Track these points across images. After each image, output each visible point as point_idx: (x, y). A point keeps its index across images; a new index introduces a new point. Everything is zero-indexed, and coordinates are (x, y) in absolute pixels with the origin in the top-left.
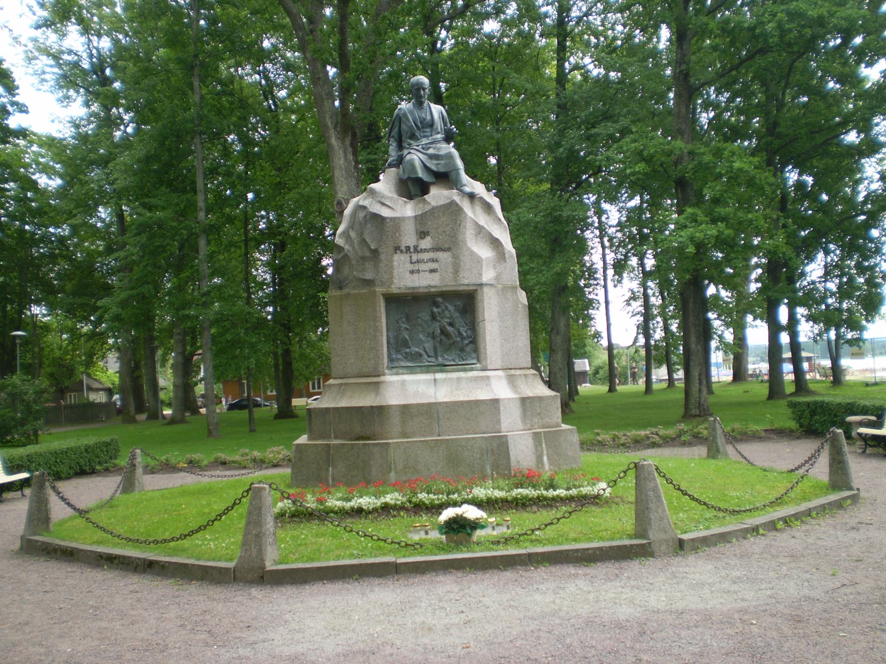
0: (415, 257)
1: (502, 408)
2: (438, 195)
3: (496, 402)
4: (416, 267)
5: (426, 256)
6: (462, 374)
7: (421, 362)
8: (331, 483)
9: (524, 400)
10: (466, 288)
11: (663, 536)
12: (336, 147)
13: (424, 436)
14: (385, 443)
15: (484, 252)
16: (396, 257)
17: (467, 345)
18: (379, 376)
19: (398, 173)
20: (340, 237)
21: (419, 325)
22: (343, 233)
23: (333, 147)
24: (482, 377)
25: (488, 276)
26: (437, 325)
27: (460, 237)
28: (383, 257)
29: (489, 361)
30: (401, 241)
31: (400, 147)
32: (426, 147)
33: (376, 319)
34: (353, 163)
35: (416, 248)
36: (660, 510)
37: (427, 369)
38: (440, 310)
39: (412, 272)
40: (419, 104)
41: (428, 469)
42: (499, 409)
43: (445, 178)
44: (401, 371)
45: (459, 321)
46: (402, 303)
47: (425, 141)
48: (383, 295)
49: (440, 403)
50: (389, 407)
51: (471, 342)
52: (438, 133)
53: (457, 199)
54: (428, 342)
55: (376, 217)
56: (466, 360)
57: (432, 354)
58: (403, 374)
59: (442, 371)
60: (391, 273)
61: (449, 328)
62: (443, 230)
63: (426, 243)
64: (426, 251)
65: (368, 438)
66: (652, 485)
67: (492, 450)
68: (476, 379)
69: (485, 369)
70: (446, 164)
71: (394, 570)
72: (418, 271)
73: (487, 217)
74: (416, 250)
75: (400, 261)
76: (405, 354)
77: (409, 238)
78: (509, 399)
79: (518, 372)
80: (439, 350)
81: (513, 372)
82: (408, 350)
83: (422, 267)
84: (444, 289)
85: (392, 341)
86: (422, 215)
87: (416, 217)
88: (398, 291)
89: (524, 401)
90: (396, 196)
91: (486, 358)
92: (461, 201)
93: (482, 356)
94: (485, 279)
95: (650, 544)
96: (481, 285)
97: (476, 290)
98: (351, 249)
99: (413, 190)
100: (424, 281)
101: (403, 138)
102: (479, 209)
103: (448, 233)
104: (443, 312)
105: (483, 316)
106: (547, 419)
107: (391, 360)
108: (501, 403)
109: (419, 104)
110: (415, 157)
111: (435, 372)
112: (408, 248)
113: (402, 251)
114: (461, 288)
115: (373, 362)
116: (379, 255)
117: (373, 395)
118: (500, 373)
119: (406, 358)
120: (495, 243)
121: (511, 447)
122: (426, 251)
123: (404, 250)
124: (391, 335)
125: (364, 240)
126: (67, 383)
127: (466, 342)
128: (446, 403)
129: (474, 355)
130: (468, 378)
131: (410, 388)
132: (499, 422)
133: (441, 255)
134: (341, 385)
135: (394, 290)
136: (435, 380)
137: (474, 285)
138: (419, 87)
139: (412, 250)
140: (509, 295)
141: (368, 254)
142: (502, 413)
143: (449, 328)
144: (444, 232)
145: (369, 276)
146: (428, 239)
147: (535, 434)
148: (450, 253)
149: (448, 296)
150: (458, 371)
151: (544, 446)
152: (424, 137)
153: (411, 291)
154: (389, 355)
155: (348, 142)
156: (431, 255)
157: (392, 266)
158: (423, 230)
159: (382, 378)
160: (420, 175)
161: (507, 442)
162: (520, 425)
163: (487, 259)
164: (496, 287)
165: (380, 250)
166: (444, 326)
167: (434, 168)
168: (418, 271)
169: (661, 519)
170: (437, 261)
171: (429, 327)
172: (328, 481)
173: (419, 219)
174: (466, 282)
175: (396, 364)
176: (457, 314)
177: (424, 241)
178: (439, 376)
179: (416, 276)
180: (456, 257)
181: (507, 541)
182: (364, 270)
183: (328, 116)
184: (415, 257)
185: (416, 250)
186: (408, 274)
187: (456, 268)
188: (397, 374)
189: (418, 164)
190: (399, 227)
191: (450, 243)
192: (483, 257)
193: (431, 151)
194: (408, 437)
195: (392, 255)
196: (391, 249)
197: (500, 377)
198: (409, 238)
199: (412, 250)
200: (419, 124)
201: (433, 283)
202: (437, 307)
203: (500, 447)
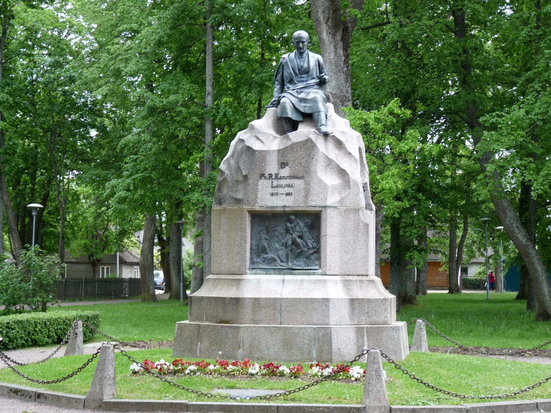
0: (275, 183)
1: (331, 306)
2: (305, 131)
3: (326, 301)
4: (275, 191)
6: (305, 277)
7: (275, 265)
8: (198, 354)
9: (352, 301)
10: (313, 209)
11: (376, 404)
12: (327, 42)
13: (269, 323)
14: (237, 327)
15: (330, 180)
16: (261, 182)
17: (312, 254)
18: (242, 274)
19: (276, 112)
20: (224, 163)
21: (276, 236)
22: (227, 160)
23: (324, 42)
24: (320, 280)
25: (332, 199)
26: (289, 236)
27: (312, 168)
28: (251, 181)
29: (328, 268)
30: (265, 170)
31: (282, 90)
32: (300, 91)
33: (244, 230)
34: (343, 58)
35: (276, 175)
36: (378, 386)
37: (280, 271)
38: (292, 225)
39: (272, 194)
40: (301, 54)
41: (268, 349)
43: (309, 117)
44: (259, 272)
45: (307, 235)
46: (263, 219)
47: (301, 85)
48: (249, 211)
49: (283, 299)
50: (244, 299)
51: (315, 252)
52: (314, 78)
53: (313, 137)
54: (282, 250)
55: (249, 148)
56: (311, 266)
57: (285, 260)
58: (260, 274)
59: (290, 274)
60: (256, 195)
61: (299, 240)
62: (298, 160)
63: (285, 172)
64: (284, 178)
65: (227, 322)
66: (375, 367)
67: (319, 338)
68: (316, 281)
69: (324, 274)
70: (311, 107)
71: (186, 409)
72: (277, 194)
73: (337, 152)
74: (277, 177)
75: (264, 186)
76: (261, 258)
77: (272, 168)
78: (339, 299)
79: (356, 278)
80: (290, 256)
81: (350, 278)
82: (265, 256)
83: (280, 190)
84: (296, 209)
85: (254, 248)
86: (284, 149)
87: (279, 150)
88: (261, 209)
89: (354, 303)
90: (273, 132)
92: (316, 139)
93: (323, 264)
94: (329, 203)
95: (364, 408)
96: (325, 207)
97: (321, 211)
98: (229, 173)
99: (286, 127)
100: (281, 202)
101: (285, 82)
102: (331, 145)
103: (303, 164)
104: (295, 227)
106: (374, 317)
107: (252, 263)
108: (331, 302)
109: (301, 54)
110: (288, 100)
111: (285, 274)
112: (270, 175)
113: (265, 178)
114: (309, 209)
115: (238, 263)
116: (248, 179)
117: (235, 288)
118: (338, 278)
119: (264, 261)
120: (342, 173)
121: (334, 337)
122: (284, 178)
124: (254, 243)
125: (239, 167)
126: (100, 256)
127: (311, 252)
128: (288, 299)
129: (317, 263)
130: (309, 281)
131: (263, 285)
132: (328, 317)
133: (296, 182)
134: (215, 279)
135: (257, 208)
136: (283, 280)
137: (319, 206)
138: (299, 40)
139: (273, 177)
140: (351, 216)
141: (241, 178)
142: (331, 310)
143: (299, 240)
144: (300, 163)
145: (240, 196)
146: (287, 168)
147: (358, 328)
148: (303, 181)
149: (299, 214)
150: (303, 274)
151: (365, 338)
152: (302, 81)
153: (270, 209)
154: (251, 258)
155: (339, 37)
156: (288, 182)
157: (257, 189)
158: (283, 161)
159: (244, 277)
160: (290, 116)
161: (331, 333)
162: (347, 320)
163: (333, 186)
164: (339, 209)
165: (249, 176)
166: (295, 238)
167: (302, 110)
168: (277, 194)
169: (378, 391)
170: (292, 186)
171: (283, 238)
172: (196, 353)
173: (282, 152)
174: (314, 204)
175: (256, 266)
176: (306, 229)
177: (284, 170)
178: (288, 277)
179: (275, 197)
180: (307, 184)
181: (265, 398)
182: (237, 191)
183: (320, 11)
184: (275, 183)
185: (277, 177)
186: (269, 196)
187: (307, 193)
188: (256, 274)
189: (289, 107)
190: (265, 159)
191: (303, 174)
192: (329, 184)
193: (302, 96)
194: (257, 323)
195: (258, 181)
196: (258, 175)
197: (336, 282)
198: (272, 168)
199: (273, 177)
200: (297, 72)
201: (287, 204)
202: (291, 223)
203: (325, 337)
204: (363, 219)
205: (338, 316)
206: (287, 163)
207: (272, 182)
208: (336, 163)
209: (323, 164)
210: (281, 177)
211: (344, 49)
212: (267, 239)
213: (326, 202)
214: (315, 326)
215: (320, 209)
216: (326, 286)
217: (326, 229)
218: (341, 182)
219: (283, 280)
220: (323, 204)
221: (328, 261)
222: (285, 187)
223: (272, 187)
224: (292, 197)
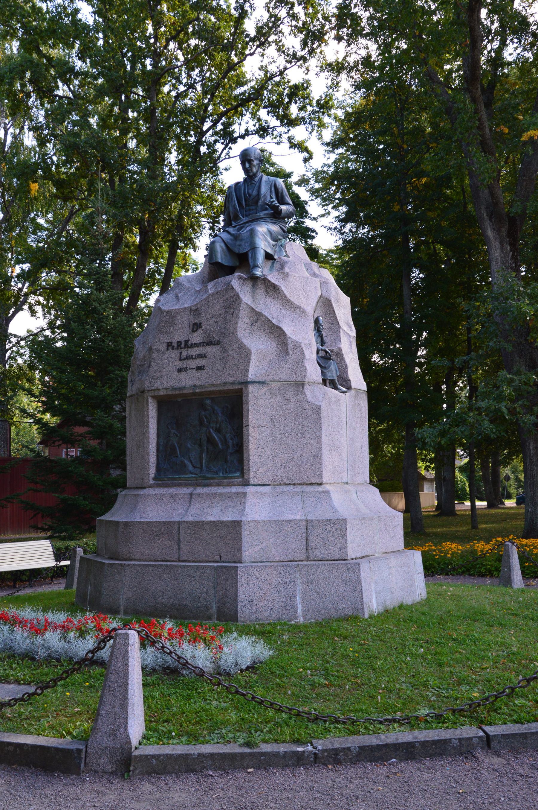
0: (185, 354)
5: (194, 352)
12: (492, 239)
23: (489, 239)
29: (252, 474)
39: (180, 370)
42: (241, 534)
56: (230, 473)
63: (197, 338)
72: (186, 369)
74: (187, 345)
76: (172, 469)
83: (193, 364)
85: (161, 448)
91: (249, 470)
105: (248, 421)
108: (244, 527)
113: (173, 348)
123: (175, 344)
139: (183, 346)
140: (290, 394)
146: (200, 332)
156: (201, 350)
160: (220, 261)
177: (196, 334)
179: (183, 374)
186: (176, 373)
199: (183, 346)
201: (198, 383)
204: (310, 398)
205: (257, 549)
206: (201, 323)
207: (181, 353)
208: (266, 318)
209: (247, 321)
210: (192, 344)
211: (511, 244)
212: (177, 436)
213: (247, 376)
214: (215, 565)
215: (240, 387)
216: (245, 503)
217: (248, 416)
218: (274, 345)
219: (191, 494)
220: (240, 378)
221: (251, 464)
222: (196, 358)
223: (180, 360)
224: (204, 372)
